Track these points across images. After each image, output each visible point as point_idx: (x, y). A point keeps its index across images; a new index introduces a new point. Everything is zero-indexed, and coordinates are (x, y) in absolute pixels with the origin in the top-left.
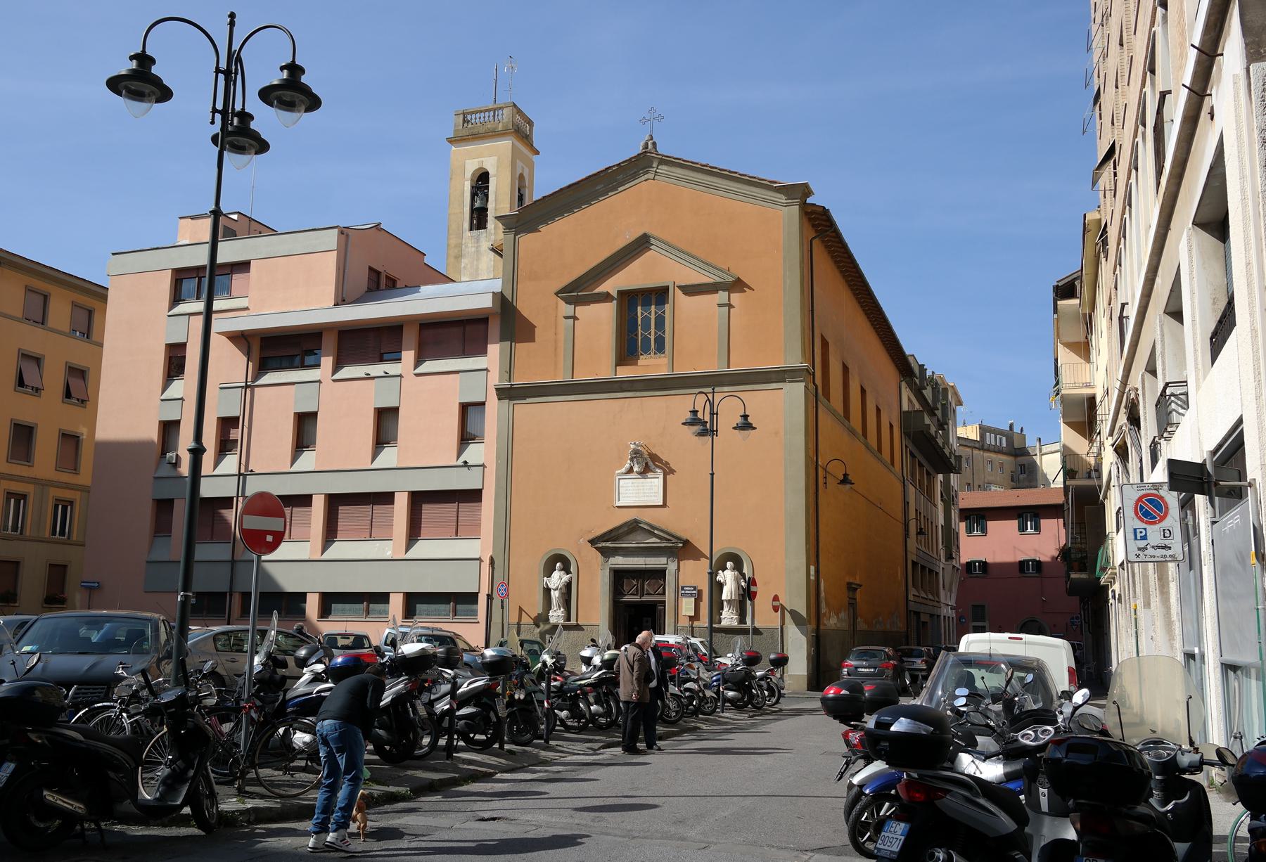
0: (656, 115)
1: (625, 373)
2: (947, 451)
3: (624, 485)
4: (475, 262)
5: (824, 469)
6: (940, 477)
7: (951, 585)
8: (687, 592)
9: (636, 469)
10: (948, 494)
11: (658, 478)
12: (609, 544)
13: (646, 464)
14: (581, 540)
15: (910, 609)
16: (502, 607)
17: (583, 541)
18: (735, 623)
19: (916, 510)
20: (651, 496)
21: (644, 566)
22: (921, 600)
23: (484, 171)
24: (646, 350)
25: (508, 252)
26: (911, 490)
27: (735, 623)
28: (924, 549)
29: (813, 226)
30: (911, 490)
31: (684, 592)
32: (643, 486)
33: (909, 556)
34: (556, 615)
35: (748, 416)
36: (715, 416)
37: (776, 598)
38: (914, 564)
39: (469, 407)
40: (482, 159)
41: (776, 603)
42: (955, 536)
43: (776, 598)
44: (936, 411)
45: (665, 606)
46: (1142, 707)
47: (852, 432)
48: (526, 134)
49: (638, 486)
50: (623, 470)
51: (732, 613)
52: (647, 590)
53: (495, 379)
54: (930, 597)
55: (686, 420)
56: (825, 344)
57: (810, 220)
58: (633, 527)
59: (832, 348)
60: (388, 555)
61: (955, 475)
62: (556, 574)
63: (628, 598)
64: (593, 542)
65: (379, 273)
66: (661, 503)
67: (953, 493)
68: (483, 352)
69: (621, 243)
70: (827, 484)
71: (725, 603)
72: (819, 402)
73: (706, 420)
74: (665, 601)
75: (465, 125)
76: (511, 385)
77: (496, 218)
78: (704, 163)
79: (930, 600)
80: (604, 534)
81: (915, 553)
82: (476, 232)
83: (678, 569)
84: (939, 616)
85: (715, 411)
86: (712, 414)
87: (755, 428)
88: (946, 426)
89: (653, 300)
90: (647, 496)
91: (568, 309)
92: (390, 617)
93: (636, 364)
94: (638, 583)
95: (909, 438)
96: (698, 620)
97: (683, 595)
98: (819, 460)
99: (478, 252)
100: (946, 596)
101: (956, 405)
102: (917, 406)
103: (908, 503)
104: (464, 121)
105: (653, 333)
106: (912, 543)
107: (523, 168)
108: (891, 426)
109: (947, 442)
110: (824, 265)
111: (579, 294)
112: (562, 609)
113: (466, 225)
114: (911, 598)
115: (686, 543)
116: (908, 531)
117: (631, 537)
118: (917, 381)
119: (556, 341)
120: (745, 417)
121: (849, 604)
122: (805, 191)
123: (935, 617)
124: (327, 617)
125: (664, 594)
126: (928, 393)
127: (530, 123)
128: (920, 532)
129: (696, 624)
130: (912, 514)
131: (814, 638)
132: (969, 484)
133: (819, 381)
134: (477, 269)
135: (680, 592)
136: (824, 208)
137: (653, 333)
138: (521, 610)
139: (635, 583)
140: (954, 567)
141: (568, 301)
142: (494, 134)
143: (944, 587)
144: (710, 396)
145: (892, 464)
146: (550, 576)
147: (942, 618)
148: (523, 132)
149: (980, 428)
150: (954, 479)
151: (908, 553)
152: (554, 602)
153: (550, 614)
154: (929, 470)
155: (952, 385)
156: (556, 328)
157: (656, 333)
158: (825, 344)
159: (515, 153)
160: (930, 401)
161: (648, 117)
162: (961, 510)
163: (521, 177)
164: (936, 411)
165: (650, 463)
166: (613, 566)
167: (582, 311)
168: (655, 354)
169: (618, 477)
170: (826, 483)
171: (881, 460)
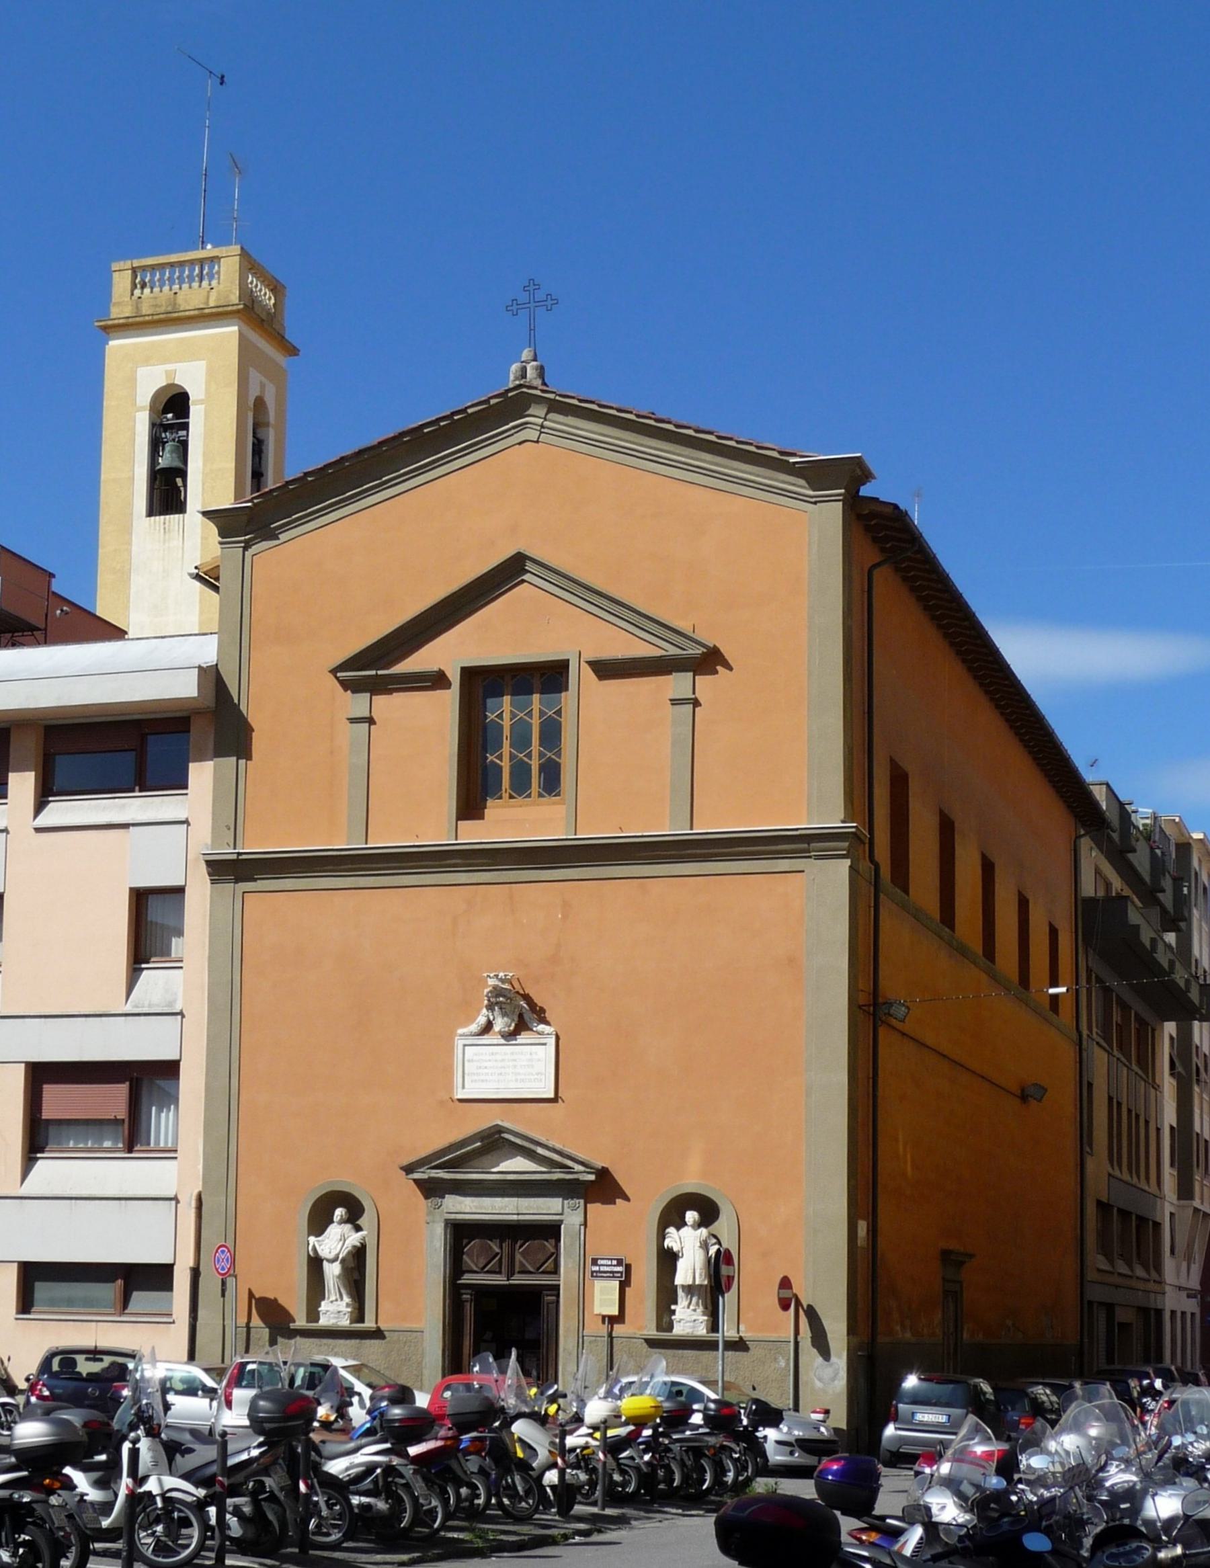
0: (540, 295)
1: (474, 834)
3: (475, 1058)
6: (1170, 1028)
7: (1190, 1246)
8: (602, 1269)
11: (545, 1044)
13: (521, 1016)
19: (1110, 1099)
20: (530, 1080)
21: (515, 1217)
22: (1119, 1280)
23: (183, 391)
24: (521, 786)
25: (228, 580)
30: (1100, 1060)
31: (596, 1268)
32: (515, 1060)
37: (785, 1283)
38: (1103, 1207)
39: (150, 896)
41: (786, 1294)
43: (785, 1283)
44: (1160, 895)
46: (1161, 1495)
49: (503, 1060)
50: (474, 1027)
51: (695, 1310)
52: (522, 1264)
54: (1140, 1272)
56: (899, 781)
57: (868, 529)
59: (914, 786)
61: (1205, 1024)
63: (467, 1279)
66: (551, 1095)
68: (179, 782)
71: (680, 1293)
72: (882, 896)
74: (559, 1285)
75: (137, 292)
76: (239, 854)
77: (206, 514)
79: (1120, 1274)
84: (1159, 1313)
88: (1183, 925)
90: (522, 1080)
91: (359, 704)
94: (501, 1248)
102: (1117, 884)
103: (1090, 1085)
104: (134, 286)
105: (535, 755)
106: (1098, 1166)
107: (263, 386)
108: (1053, 932)
111: (380, 672)
112: (347, 1299)
114: (1091, 1275)
118: (1115, 836)
123: (1152, 1317)
125: (555, 1271)
129: (618, 1329)
135: (590, 1268)
136: (896, 507)
137: (535, 755)
139: (497, 1250)
140: (1196, 1210)
143: (1172, 1252)
155: (1201, 836)
158: (899, 781)
159: (247, 357)
161: (523, 297)
163: (260, 404)
164: (1160, 895)
165: (528, 1016)
166: (453, 1216)
167: (385, 705)
168: (540, 795)
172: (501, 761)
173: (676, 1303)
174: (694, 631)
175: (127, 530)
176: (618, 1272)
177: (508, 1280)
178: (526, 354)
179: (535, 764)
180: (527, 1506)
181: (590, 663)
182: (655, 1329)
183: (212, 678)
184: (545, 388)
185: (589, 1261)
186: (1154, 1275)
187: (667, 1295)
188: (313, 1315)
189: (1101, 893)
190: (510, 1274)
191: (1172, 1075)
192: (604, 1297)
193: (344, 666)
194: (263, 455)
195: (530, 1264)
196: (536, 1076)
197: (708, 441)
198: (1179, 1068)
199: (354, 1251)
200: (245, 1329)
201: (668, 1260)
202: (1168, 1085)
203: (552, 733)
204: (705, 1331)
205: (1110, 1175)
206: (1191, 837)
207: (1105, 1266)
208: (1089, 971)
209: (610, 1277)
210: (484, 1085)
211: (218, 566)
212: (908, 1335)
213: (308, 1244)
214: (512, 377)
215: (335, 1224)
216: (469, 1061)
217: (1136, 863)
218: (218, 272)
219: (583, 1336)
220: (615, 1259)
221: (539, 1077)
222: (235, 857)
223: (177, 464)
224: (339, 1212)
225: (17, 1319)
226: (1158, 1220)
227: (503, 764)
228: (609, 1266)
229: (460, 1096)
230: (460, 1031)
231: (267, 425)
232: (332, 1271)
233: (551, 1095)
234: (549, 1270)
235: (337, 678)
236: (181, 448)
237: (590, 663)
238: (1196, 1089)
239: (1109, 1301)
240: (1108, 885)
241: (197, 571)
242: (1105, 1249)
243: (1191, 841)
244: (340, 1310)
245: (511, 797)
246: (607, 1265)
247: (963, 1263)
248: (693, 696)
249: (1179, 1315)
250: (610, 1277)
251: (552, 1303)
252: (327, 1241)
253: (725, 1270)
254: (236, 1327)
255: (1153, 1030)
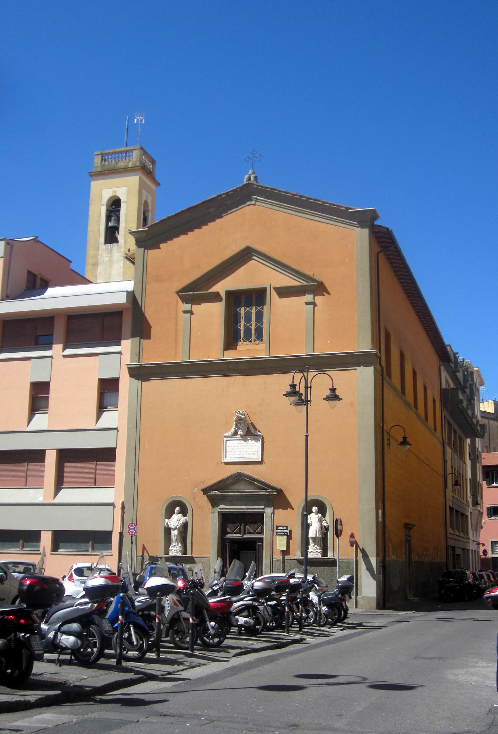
1: (231, 356)
2: (474, 421)
4: (108, 269)
5: (388, 433)
6: (468, 441)
9: (240, 432)
10: (475, 454)
12: (217, 493)
13: (248, 428)
14: (195, 489)
15: (448, 544)
16: (132, 543)
17: (198, 491)
18: (319, 556)
19: (452, 467)
21: (246, 510)
22: (456, 538)
24: (248, 337)
25: (139, 260)
26: (448, 450)
27: (319, 556)
28: (457, 497)
29: (379, 242)
30: (448, 450)
31: (278, 531)
32: (246, 446)
33: (447, 503)
34: (175, 550)
35: (336, 389)
36: (309, 389)
37: (352, 536)
38: (451, 508)
40: (115, 189)
41: (352, 540)
42: (480, 487)
43: (352, 536)
45: (263, 542)
47: (407, 404)
48: (150, 171)
50: (230, 433)
52: (248, 530)
53: (127, 359)
54: (462, 535)
55: (287, 392)
56: (388, 336)
57: (376, 237)
58: (238, 478)
60: (40, 500)
62: (175, 517)
63: (229, 536)
64: (205, 491)
65: (35, 276)
66: (260, 460)
67: (477, 453)
69: (228, 254)
70: (390, 445)
71: (311, 540)
73: (301, 392)
75: (103, 163)
78: (295, 193)
79: (457, 535)
80: (215, 485)
81: (451, 500)
82: (109, 246)
83: (273, 513)
84: (468, 550)
85: (309, 386)
86: (307, 387)
87: (341, 399)
89: (243, 301)
92: (41, 551)
93: (236, 349)
95: (447, 410)
96: (289, 554)
97: (277, 533)
98: (385, 426)
99: (111, 261)
100: (473, 534)
101: (480, 385)
102: (452, 385)
103: (446, 461)
104: (102, 160)
105: (253, 325)
107: (147, 197)
109: (473, 414)
110: (386, 273)
112: (180, 545)
113: (102, 239)
114: (449, 536)
115: (280, 492)
116: (447, 483)
117: (236, 486)
118: (453, 365)
119: (176, 330)
120: (333, 390)
121: (406, 540)
122: (374, 215)
124: (57, 551)
125: (261, 532)
126: (460, 375)
127: (153, 162)
128: (456, 483)
130: (449, 470)
131: (382, 567)
132: (487, 447)
133: (383, 363)
134: (110, 274)
135: (275, 530)
136: (388, 229)
137: (253, 325)
138: (144, 548)
141: (185, 300)
142: (126, 171)
144: (305, 374)
145: (435, 429)
146: (170, 518)
147: (474, 551)
148: (148, 169)
149: (494, 404)
150: (478, 441)
151: (447, 501)
152: (173, 538)
153: (171, 548)
154: (460, 435)
155: (477, 369)
156: (176, 319)
157: (256, 325)
159: (142, 185)
160: (462, 384)
162: (484, 467)
163: (146, 203)
167: (196, 308)
168: (255, 341)
169: (225, 439)
170: (389, 444)
171: (427, 426)
172: (241, 327)
173: (309, 545)
174: (314, 276)
175: (97, 249)
176: (286, 532)
177: (243, 536)
178: (250, 172)
179: (253, 328)
180: (151, 639)
181: (275, 289)
182: (301, 555)
183: (131, 296)
184: (257, 184)
185: (275, 528)
186: (466, 536)
187: (306, 541)
188: (167, 551)
189: (447, 388)
190: (244, 533)
191: (469, 459)
192: (281, 543)
193: (183, 290)
194: (147, 222)
195: (252, 529)
196: (254, 453)
197: (319, 204)
198: (472, 457)
199: (183, 525)
200: (141, 558)
201: (306, 526)
202: (468, 462)
203: (260, 316)
204: (320, 556)
205: (453, 496)
206: (473, 369)
207: (452, 532)
208: (445, 417)
209: (283, 534)
210: (234, 456)
211: (134, 253)
212: (395, 557)
213: (165, 522)
214: (245, 180)
215: (176, 514)
216: (228, 446)
217: (458, 376)
218: (132, 155)
219: (273, 559)
220: (285, 527)
221: (255, 453)
222: (139, 366)
223: (116, 225)
224: (177, 509)
225: (51, 554)
226: (467, 515)
227: (241, 328)
228: (283, 529)
229: (224, 461)
230: (225, 434)
231: (148, 211)
232: (174, 533)
233: (260, 460)
234: (259, 532)
235: (179, 295)
236: (117, 219)
237: (275, 289)
238: (478, 465)
239: (453, 546)
240: (449, 385)
241: (126, 255)
242: (452, 527)
243: (473, 371)
244: (177, 549)
245: (244, 341)
246: (282, 529)
247: (411, 528)
248: (314, 301)
249: (474, 551)
250: (283, 534)
251: (260, 546)
252: (172, 521)
253: (339, 527)
254: (137, 557)
255: (464, 441)
